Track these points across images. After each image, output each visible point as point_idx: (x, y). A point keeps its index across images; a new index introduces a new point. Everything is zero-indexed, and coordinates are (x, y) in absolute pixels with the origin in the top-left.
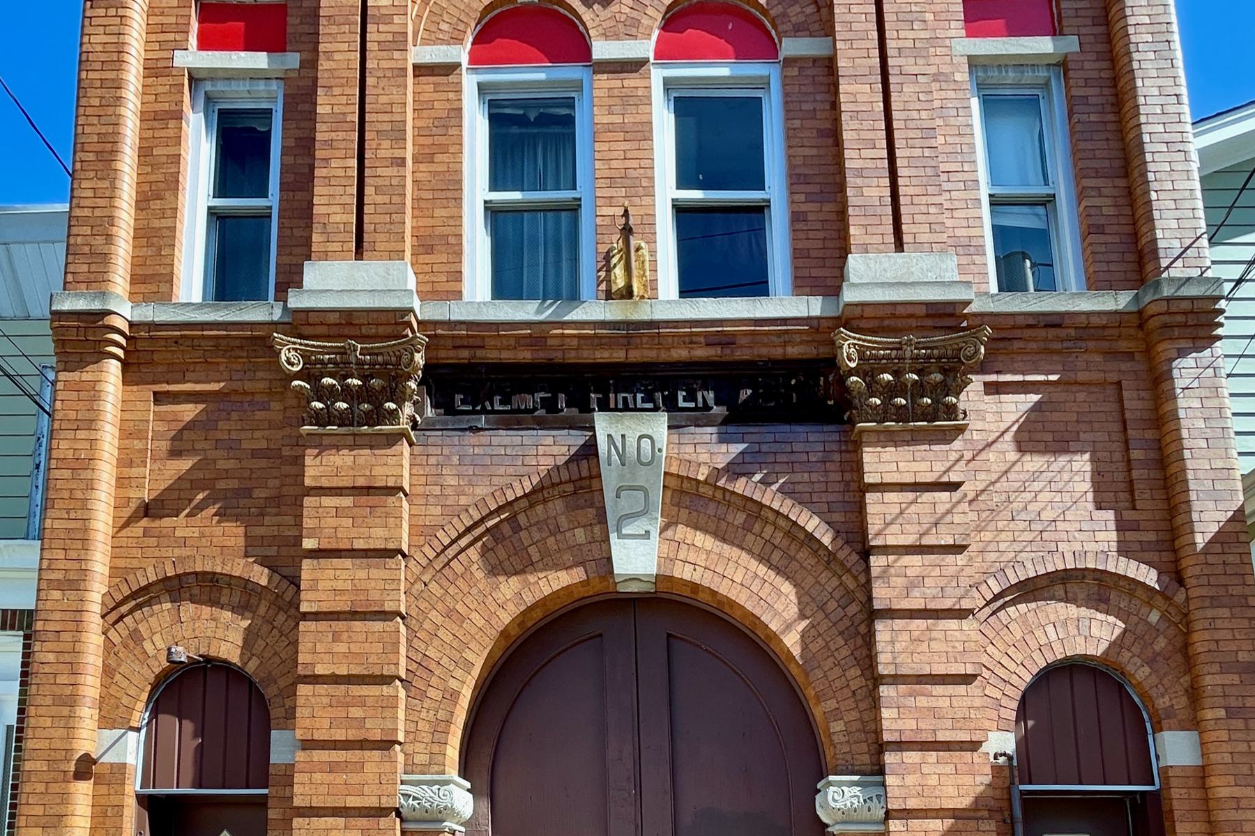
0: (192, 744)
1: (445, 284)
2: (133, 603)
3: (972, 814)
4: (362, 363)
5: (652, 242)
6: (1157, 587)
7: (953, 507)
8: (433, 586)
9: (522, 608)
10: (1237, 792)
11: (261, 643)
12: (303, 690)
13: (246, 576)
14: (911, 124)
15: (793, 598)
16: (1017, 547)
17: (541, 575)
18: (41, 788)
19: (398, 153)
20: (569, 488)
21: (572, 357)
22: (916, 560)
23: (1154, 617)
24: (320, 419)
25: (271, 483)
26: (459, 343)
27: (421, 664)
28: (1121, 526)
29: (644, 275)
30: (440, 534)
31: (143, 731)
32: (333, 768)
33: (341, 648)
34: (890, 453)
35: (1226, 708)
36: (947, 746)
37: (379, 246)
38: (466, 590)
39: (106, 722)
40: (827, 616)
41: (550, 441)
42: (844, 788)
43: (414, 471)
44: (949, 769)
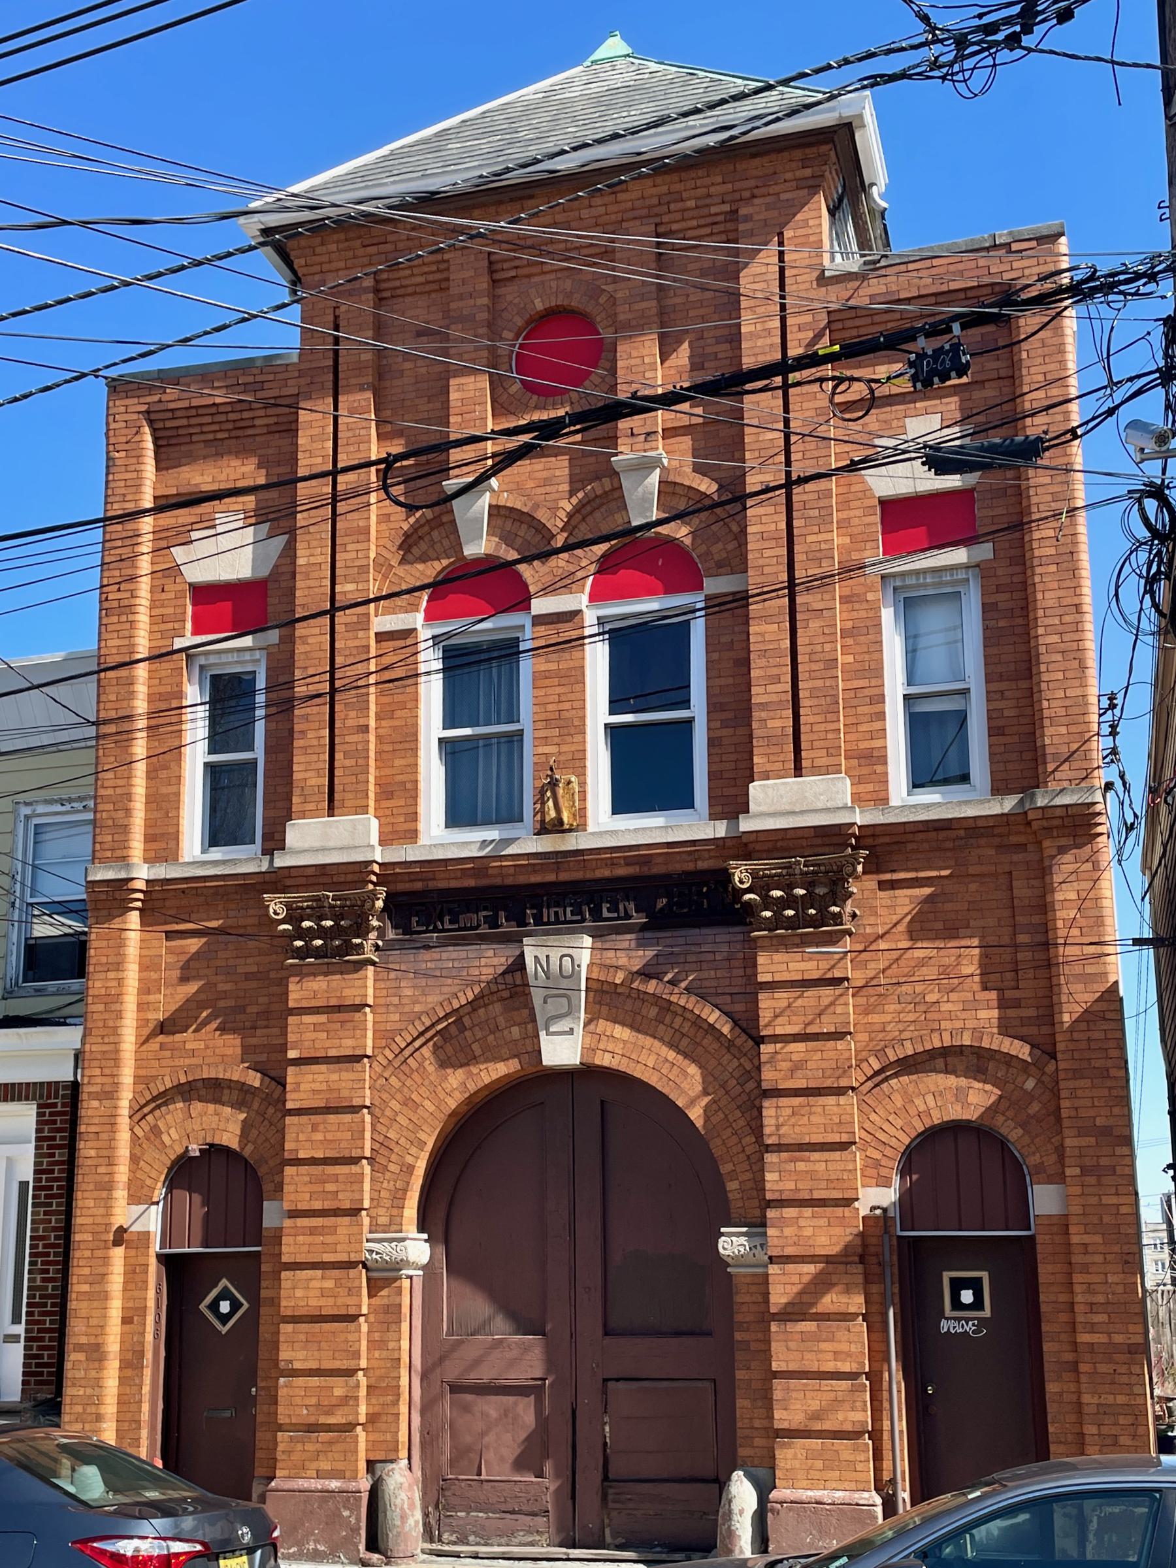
0: (200, 1211)
1: (401, 829)
2: (154, 1105)
3: (844, 1259)
4: (335, 907)
5: (582, 773)
6: (1029, 1060)
7: (836, 999)
8: (393, 1080)
9: (467, 1095)
10: (1087, 1239)
11: (254, 1132)
12: (289, 1170)
13: (242, 1080)
14: (814, 657)
15: (698, 1078)
16: (901, 1027)
17: (482, 1067)
18: (88, 1253)
19: (362, 722)
20: (506, 994)
21: (509, 881)
22: (800, 1047)
23: (1030, 1084)
24: (301, 954)
25: (261, 1000)
26: (413, 877)
27: (383, 1144)
28: (1002, 1004)
29: (573, 805)
30: (398, 1039)
31: (161, 1204)
32: (313, 1231)
33: (319, 1136)
34: (779, 957)
35: (1081, 1167)
36: (823, 1203)
37: (348, 803)
38: (419, 1081)
39: (133, 1199)
40: (727, 1093)
41: (490, 953)
42: (734, 1239)
43: (378, 985)
44: (823, 1222)
